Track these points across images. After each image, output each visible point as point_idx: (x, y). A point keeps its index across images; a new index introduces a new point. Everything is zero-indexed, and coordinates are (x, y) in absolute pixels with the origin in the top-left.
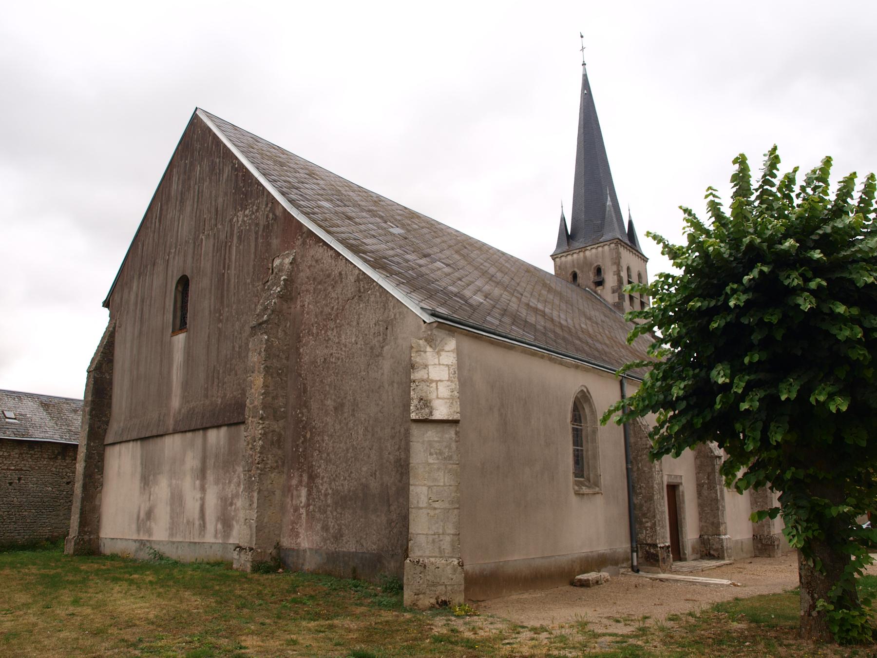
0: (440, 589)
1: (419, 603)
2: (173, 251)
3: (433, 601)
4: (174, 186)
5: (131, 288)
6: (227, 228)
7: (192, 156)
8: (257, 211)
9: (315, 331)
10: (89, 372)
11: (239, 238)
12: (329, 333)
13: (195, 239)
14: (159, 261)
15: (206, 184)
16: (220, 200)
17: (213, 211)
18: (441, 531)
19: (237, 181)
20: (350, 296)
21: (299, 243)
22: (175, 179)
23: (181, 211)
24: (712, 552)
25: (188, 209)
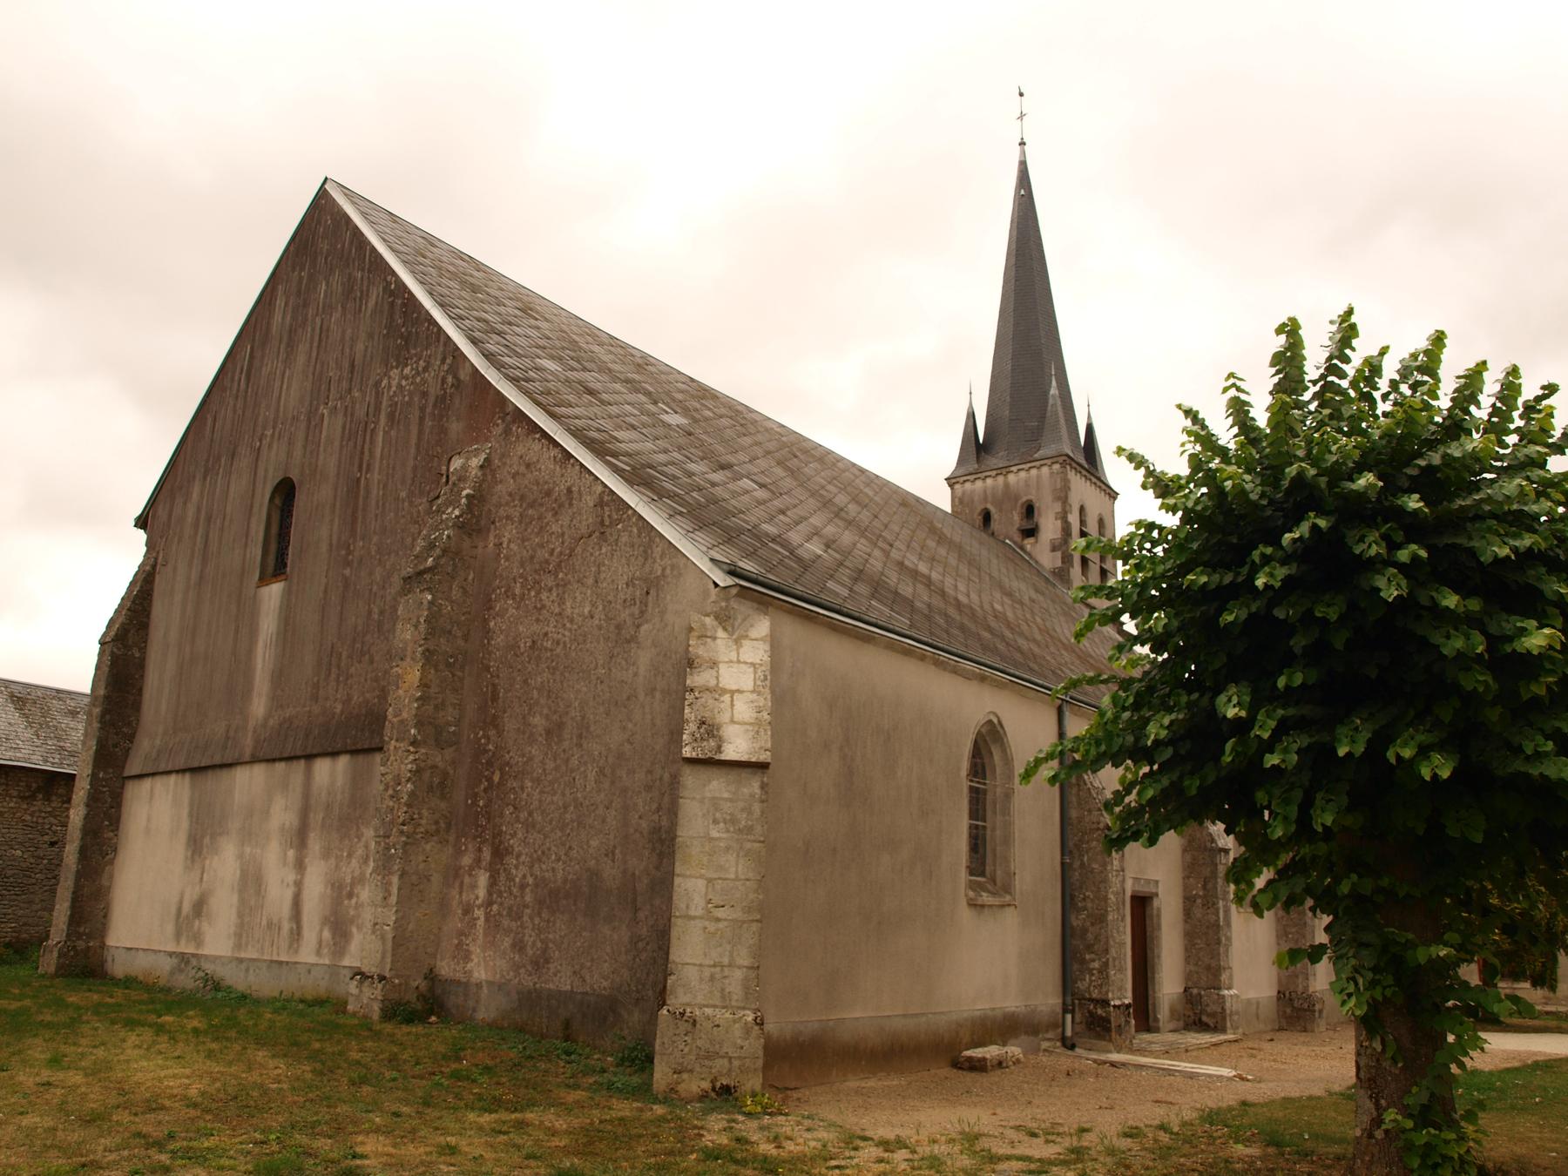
0: (720, 1064)
2: (269, 433)
3: (706, 1085)
8: (426, 369)
9: (517, 591)
10: (102, 643)
12: (544, 596)
15: (336, 315)
16: (360, 347)
17: (346, 365)
19: (391, 315)
20: (584, 530)
22: (280, 302)
24: (1204, 1018)
25: (301, 359)
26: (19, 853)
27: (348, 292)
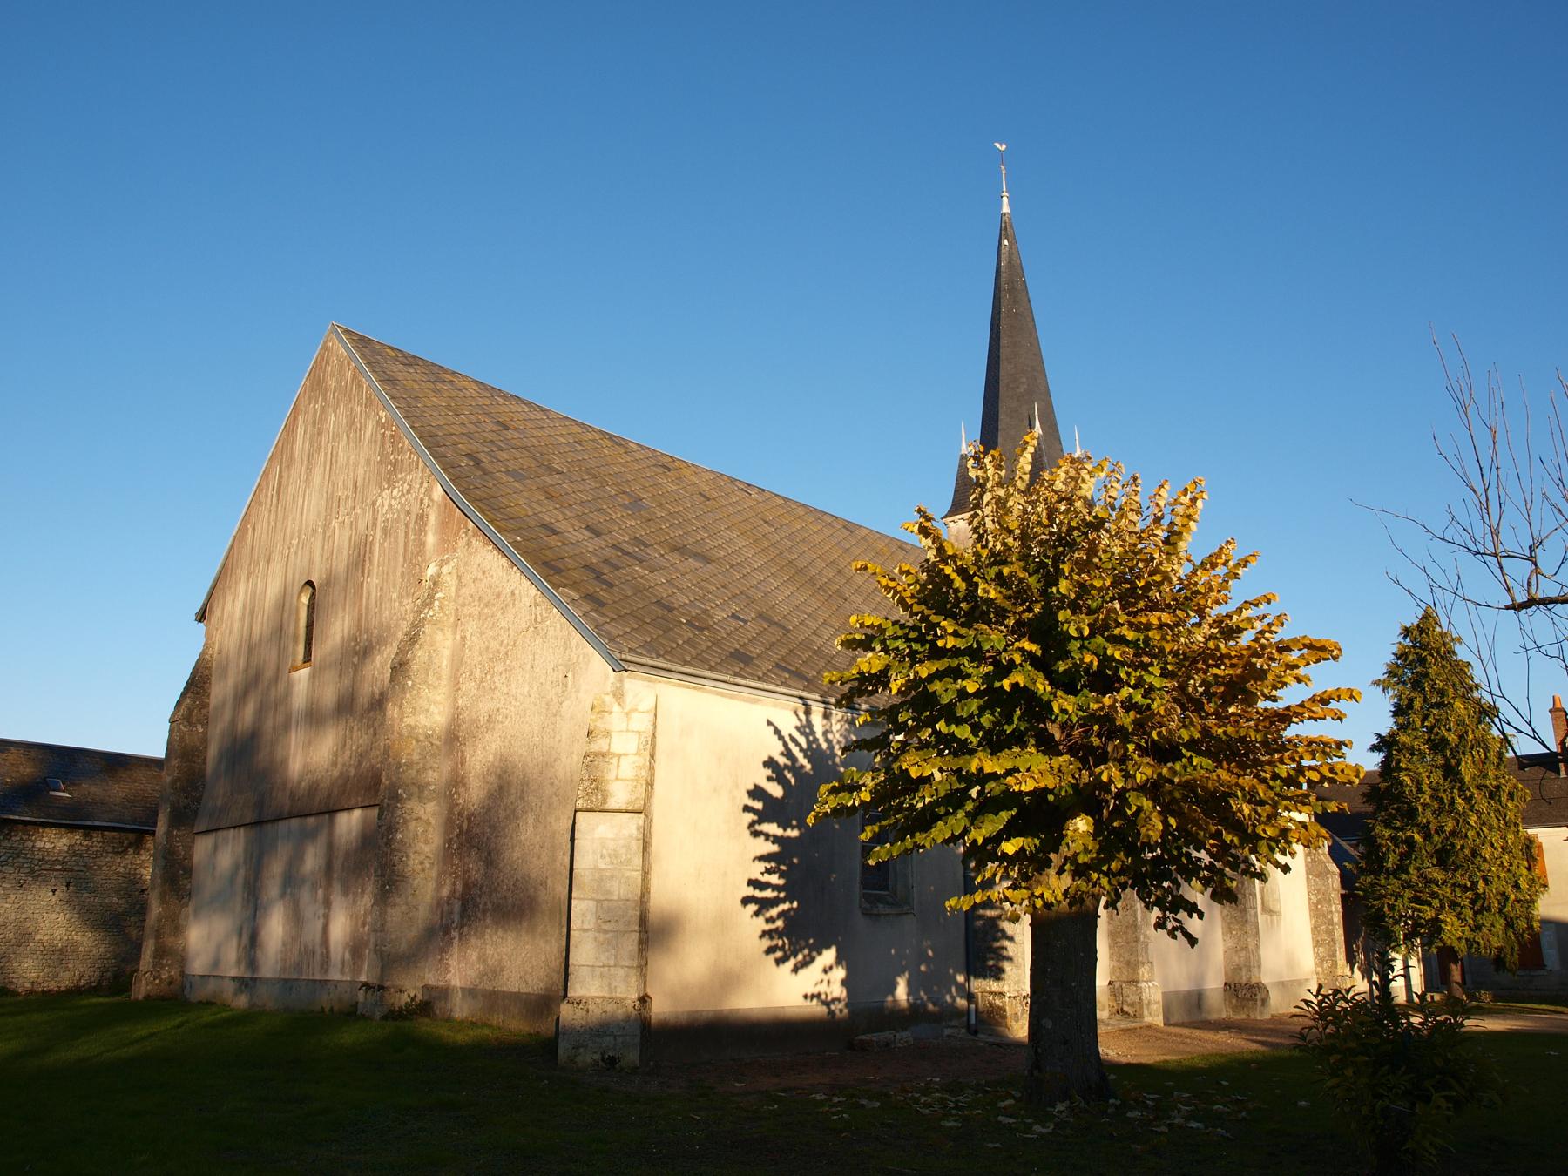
0: (608, 1040)
1: (579, 1059)
2: (295, 542)
3: (597, 1057)
4: (299, 443)
5: (235, 596)
6: (369, 515)
7: (324, 399)
8: (409, 491)
9: (478, 675)
10: (172, 722)
11: (384, 530)
12: (496, 678)
13: (326, 527)
14: (276, 557)
15: (343, 443)
16: (361, 471)
17: (351, 486)
18: (612, 962)
19: (383, 444)
20: (524, 626)
21: (462, 543)
22: (300, 430)
23: (308, 481)
24: (1126, 1008)
25: (317, 480)
26: (115, 900)
27: (351, 423)
